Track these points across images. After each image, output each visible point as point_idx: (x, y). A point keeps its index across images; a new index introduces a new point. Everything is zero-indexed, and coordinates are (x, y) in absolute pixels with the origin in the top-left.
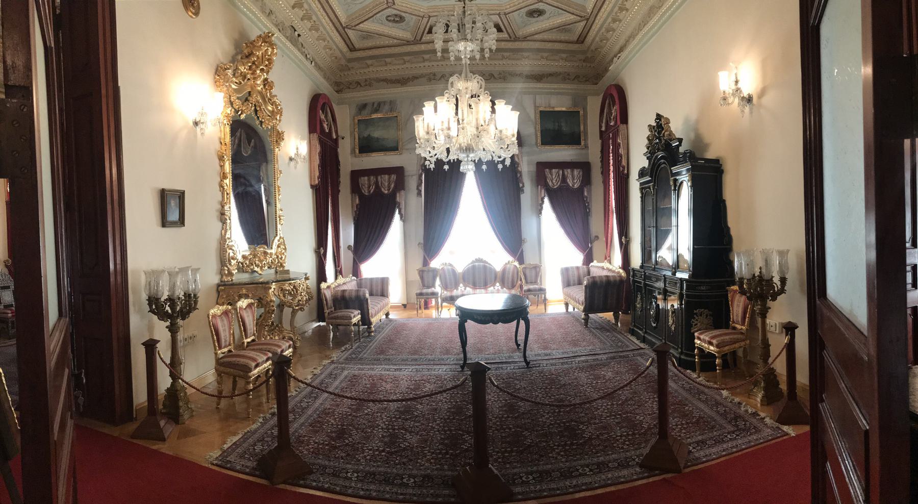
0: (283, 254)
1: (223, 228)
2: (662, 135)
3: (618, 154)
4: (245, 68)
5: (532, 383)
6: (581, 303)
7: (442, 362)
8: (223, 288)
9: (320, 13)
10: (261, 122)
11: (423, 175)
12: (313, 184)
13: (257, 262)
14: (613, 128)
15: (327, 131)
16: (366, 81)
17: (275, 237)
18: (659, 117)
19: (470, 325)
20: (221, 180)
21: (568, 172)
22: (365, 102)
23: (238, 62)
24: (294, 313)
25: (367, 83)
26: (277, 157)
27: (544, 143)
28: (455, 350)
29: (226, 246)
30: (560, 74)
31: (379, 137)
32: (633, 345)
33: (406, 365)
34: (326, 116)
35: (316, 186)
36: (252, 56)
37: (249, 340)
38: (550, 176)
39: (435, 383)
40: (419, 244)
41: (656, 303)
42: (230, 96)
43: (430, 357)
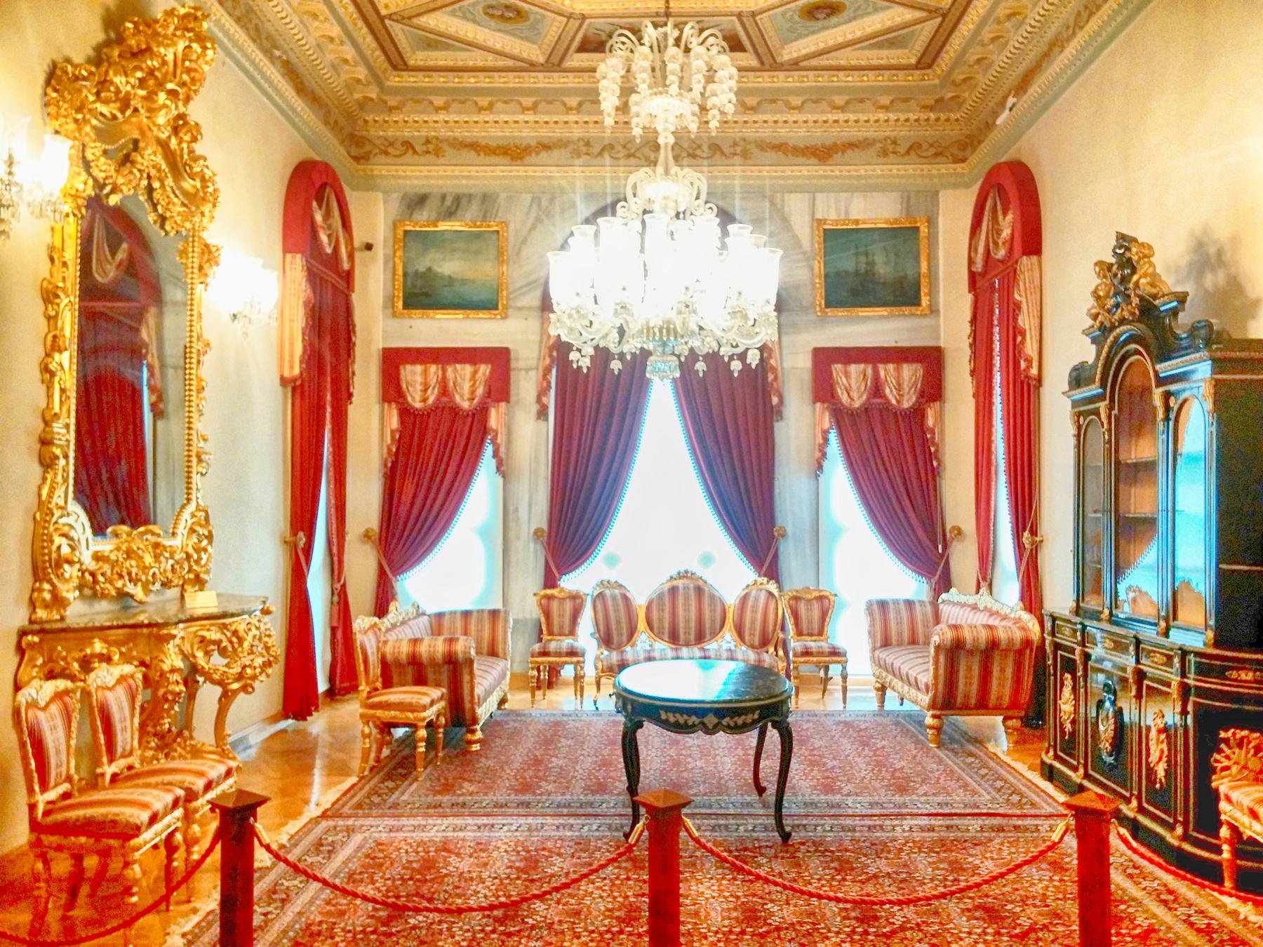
0: (205, 550)
1: (44, 479)
2: (1131, 285)
3: (1014, 328)
4: (128, 82)
5: (813, 914)
6: (922, 686)
7: (590, 810)
8: (36, 639)
10: (163, 219)
11: (554, 371)
12: (286, 374)
13: (134, 571)
14: (1001, 267)
16: (735, 144)
17: (183, 507)
18: (1124, 241)
19: (651, 737)
20: (48, 355)
21: (887, 371)
22: (423, 191)
23: (110, 65)
24: (226, 698)
25: (431, 147)
26: (199, 305)
28: (617, 784)
29: (52, 528)
30: (874, 141)
31: (454, 276)
32: (1049, 804)
33: (504, 815)
34: (327, 216)
35: (294, 380)
36: (147, 54)
37: (52, 795)
38: (844, 380)
39: (573, 856)
41: (1114, 703)
42: (84, 146)
43: (560, 798)
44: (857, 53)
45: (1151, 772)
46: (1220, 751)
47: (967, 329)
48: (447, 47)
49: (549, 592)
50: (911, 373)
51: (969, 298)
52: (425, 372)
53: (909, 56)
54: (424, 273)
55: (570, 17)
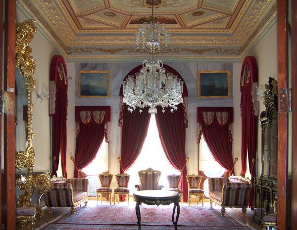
9: (62, 6)
12: (50, 113)
15: (61, 80)
16: (88, 49)
21: (218, 114)
34: (61, 70)
40: (119, 158)
47: (240, 102)
50: (225, 114)
52: (87, 113)
53: (223, 25)
54: (86, 86)
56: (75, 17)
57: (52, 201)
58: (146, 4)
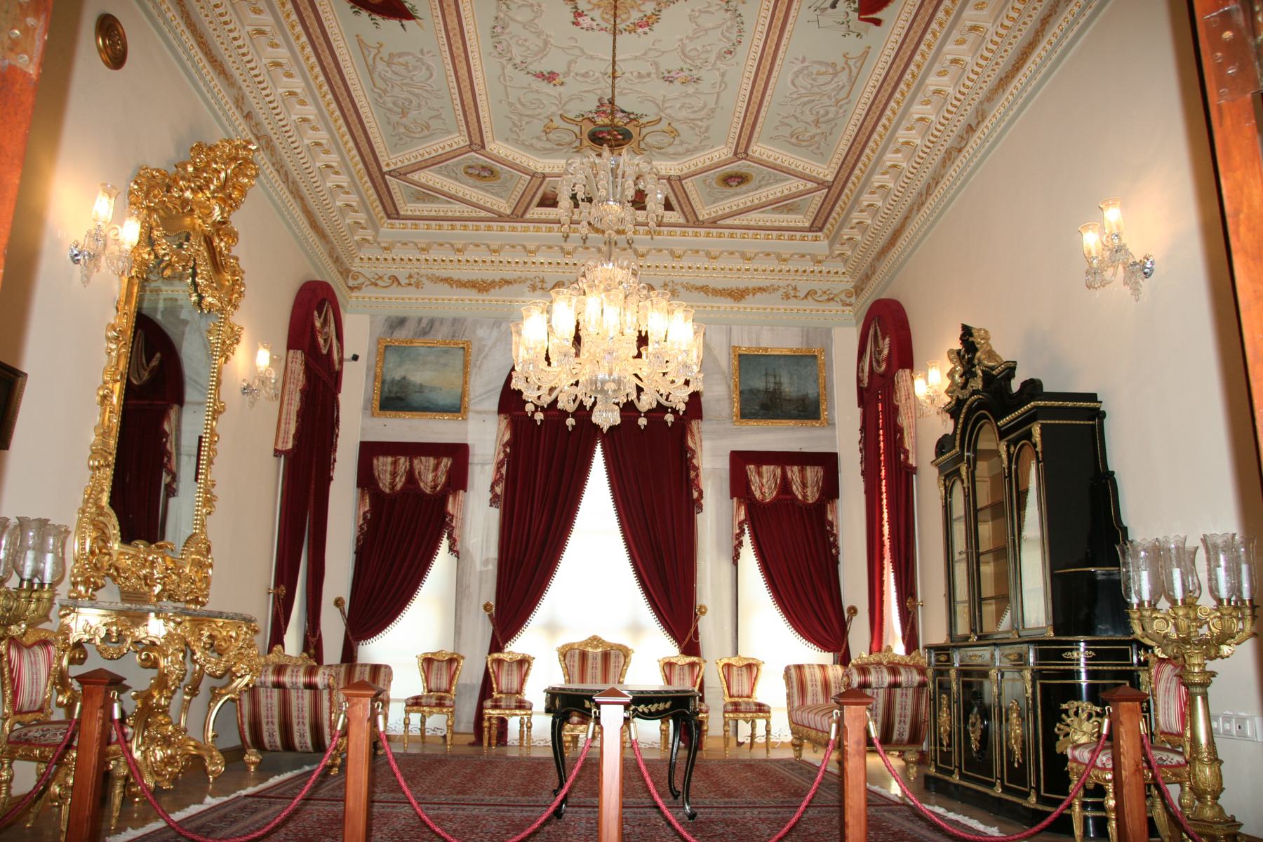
12: (280, 447)
16: (410, 276)
21: (794, 472)
27: (745, 414)
30: (778, 289)
35: (286, 453)
44: (762, 216)
45: (1010, 752)
46: (1062, 721)
47: (858, 436)
48: (433, 199)
49: (496, 655)
50: (813, 474)
51: (858, 412)
52: (395, 464)
53: (801, 220)
54: (399, 381)
55: (533, 175)
56: (378, 176)
57: (265, 727)
58: (587, 142)
